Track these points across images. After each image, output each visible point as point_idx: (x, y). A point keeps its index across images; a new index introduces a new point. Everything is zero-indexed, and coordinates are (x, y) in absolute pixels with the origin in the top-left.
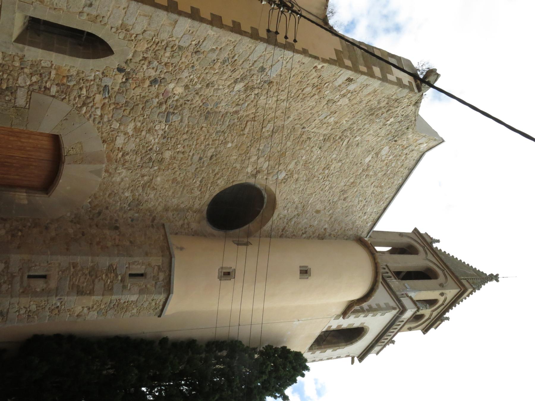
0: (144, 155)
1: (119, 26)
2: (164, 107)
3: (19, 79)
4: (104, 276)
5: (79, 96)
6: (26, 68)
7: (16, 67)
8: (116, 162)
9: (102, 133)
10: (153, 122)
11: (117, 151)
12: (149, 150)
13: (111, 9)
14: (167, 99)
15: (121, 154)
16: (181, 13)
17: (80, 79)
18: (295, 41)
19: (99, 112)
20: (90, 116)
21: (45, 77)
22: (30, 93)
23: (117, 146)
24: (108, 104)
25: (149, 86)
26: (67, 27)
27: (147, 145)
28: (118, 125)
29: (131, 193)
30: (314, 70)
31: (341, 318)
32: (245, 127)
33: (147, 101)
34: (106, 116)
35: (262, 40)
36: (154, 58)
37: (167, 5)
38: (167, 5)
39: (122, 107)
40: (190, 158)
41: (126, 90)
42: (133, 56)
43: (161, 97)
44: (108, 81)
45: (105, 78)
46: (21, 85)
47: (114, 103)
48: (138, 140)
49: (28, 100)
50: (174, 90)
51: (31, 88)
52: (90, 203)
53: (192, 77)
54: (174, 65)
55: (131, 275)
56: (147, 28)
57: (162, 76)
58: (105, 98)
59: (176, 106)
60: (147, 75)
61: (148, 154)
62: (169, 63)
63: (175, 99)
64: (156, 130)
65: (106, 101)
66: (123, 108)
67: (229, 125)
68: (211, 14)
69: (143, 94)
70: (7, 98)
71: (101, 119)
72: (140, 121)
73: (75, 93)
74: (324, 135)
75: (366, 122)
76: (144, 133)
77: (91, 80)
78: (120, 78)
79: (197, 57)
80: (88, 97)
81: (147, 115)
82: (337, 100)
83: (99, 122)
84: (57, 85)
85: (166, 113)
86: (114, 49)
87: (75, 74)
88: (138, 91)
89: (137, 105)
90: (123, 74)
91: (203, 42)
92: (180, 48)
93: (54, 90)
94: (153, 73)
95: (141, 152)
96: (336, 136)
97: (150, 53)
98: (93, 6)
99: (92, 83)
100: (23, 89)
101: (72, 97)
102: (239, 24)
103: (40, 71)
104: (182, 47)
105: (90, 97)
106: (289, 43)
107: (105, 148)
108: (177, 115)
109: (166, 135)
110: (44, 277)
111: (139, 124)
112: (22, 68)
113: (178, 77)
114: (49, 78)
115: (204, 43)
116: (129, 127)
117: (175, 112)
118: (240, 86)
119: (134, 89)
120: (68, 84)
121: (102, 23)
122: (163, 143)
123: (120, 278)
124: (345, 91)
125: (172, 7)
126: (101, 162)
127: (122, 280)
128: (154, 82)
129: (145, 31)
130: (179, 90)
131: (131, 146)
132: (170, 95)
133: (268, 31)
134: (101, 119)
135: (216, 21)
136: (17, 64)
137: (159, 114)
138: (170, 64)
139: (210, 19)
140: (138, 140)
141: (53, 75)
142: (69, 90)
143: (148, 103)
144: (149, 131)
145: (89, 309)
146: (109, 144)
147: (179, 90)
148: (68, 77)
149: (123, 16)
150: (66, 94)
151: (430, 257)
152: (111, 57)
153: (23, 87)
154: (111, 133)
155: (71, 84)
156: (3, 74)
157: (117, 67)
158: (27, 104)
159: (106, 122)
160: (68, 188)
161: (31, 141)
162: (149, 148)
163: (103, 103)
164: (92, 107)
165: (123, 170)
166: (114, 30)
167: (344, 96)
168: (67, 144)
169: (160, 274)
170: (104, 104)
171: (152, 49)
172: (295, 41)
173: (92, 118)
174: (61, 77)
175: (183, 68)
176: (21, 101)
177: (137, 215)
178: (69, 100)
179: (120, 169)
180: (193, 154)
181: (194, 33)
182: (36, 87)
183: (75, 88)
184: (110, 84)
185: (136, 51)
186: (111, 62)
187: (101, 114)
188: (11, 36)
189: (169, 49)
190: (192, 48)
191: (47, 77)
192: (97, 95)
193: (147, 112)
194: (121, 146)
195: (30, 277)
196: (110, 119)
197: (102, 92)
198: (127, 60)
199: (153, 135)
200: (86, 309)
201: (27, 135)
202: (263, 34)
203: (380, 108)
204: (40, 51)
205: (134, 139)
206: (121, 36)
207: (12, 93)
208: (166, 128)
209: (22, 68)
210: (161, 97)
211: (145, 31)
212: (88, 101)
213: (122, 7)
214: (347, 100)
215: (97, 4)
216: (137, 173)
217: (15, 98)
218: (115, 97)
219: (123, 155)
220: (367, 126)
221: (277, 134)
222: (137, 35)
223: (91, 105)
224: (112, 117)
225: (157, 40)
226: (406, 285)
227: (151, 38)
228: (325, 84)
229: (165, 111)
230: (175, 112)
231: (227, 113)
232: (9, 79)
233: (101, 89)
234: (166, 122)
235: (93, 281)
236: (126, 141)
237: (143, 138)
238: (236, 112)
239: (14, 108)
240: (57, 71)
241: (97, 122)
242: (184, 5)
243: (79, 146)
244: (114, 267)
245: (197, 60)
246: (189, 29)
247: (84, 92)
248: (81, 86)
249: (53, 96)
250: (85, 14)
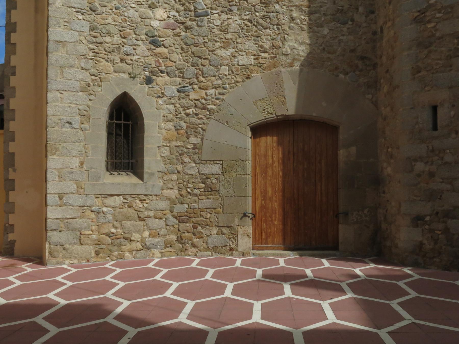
0: (260, 27)
1: (86, 93)
2: (189, 23)
3: (190, 173)
4: (430, 26)
5: (197, 115)
6: (177, 168)
7: (178, 177)
8: (276, 57)
9: (237, 82)
10: (211, 29)
11: (260, 60)
12: (251, 23)
13: (66, 105)
14: (179, 23)
15: (263, 55)
17: (177, 118)
19: (212, 92)
20: (217, 99)
21: (182, 150)
22: (203, 162)
23: (253, 62)
24: (199, 84)
25: (165, 47)
27: (245, 27)
28: (223, 67)
29: (322, 26)
33: (186, 44)
34: (215, 83)
36: (119, 51)
39: (199, 69)
41: (178, 69)
42: (124, 73)
43: (178, 30)
44: (172, 90)
45: (166, 94)
47: (197, 78)
48: (239, 40)
49: (212, 162)
50: (161, 19)
51: (198, 161)
52: (346, 74)
53: (133, 5)
54: (121, 29)
56: (78, 68)
57: (143, 37)
58: (193, 88)
59: (185, 10)
60: (147, 53)
61: (257, 22)
62: (121, 35)
63: (177, 14)
64: (222, 23)
65: (196, 87)
66: (201, 67)
69: (179, 51)
70: (214, 182)
71: (220, 87)
72: (214, 45)
73: (194, 120)
76: (229, 36)
77: (175, 107)
79: (100, 8)
80: (196, 106)
81: (204, 39)
83: (224, 88)
84: (188, 139)
85: (197, 19)
87: (171, 123)
88: (175, 57)
89: (193, 53)
91: (74, 8)
92: (92, 29)
93: (193, 140)
94: (143, 48)
95: (256, 32)
97: (112, 58)
98: (69, 120)
99: (178, 105)
100: (201, 169)
101: (199, 121)
103: (177, 156)
104: (90, 27)
105: (195, 104)
107: (258, 74)
108: (197, 6)
109: (226, 9)
111: (218, 44)
113: (140, 20)
114: (183, 147)
115: (75, 6)
116: (224, 55)
119: (175, 62)
120: (185, 128)
121: (88, 109)
122: (238, 9)
126: (279, 74)
128: (155, 43)
129: (83, 69)
130: (160, 13)
131: (251, 46)
132: (172, 21)
134: (220, 87)
136: (175, 177)
138: (122, 33)
140: (239, 40)
141: (179, 144)
142: (191, 126)
143: (188, 42)
144: (225, 31)
146: (252, 71)
148: (177, 130)
149: (71, 93)
150: (196, 129)
152: (132, 93)
153: (199, 169)
154: (235, 73)
156: (188, 188)
157: (145, 85)
158: (217, 163)
159: (223, 82)
160: (324, 104)
161: (270, 153)
162: (249, 24)
163: (199, 90)
164: (205, 100)
165: (286, 46)
166: (92, 97)
168: (259, 116)
170: (200, 88)
171: (106, 56)
173: (221, 97)
174: (178, 135)
175: (123, 18)
176: (216, 169)
177: (361, 9)
178: (204, 123)
179: (284, 50)
181: (67, 20)
182: (196, 157)
183: (188, 121)
184: (174, 88)
185: (115, 71)
186: (139, 93)
187: (213, 88)
188: (135, 185)
189: (99, 40)
190: (88, 16)
191: (181, 148)
192: (191, 97)
193: (201, 40)
194: (253, 57)
195: (435, 128)
196: (217, 77)
197: (186, 93)
198: (131, 77)
199: (229, 24)
201: (263, 158)
205: (239, 46)
207: (208, 178)
208: (217, 12)
209: (178, 172)
210: (178, 30)
211: (83, 69)
212: (199, 105)
213: (60, 95)
215: (65, 117)
216: (289, 27)
217: (213, 174)
218: (190, 79)
219: (265, 52)
222: (91, 75)
223: (204, 101)
224: (214, 76)
225: (91, 54)
227: (90, 61)
229: (194, 20)
230: (192, 8)
232: (193, 182)
233: (183, 95)
234: (208, 15)
235: (439, 38)
236: (244, 53)
237: (235, 35)
239: (225, 174)
240: (172, 140)
241: (224, 91)
243: (259, 103)
244: (417, 14)
245: (105, 6)
246: (62, 27)
247: (190, 111)
248: (185, 116)
249: (202, 139)
250: (82, 126)
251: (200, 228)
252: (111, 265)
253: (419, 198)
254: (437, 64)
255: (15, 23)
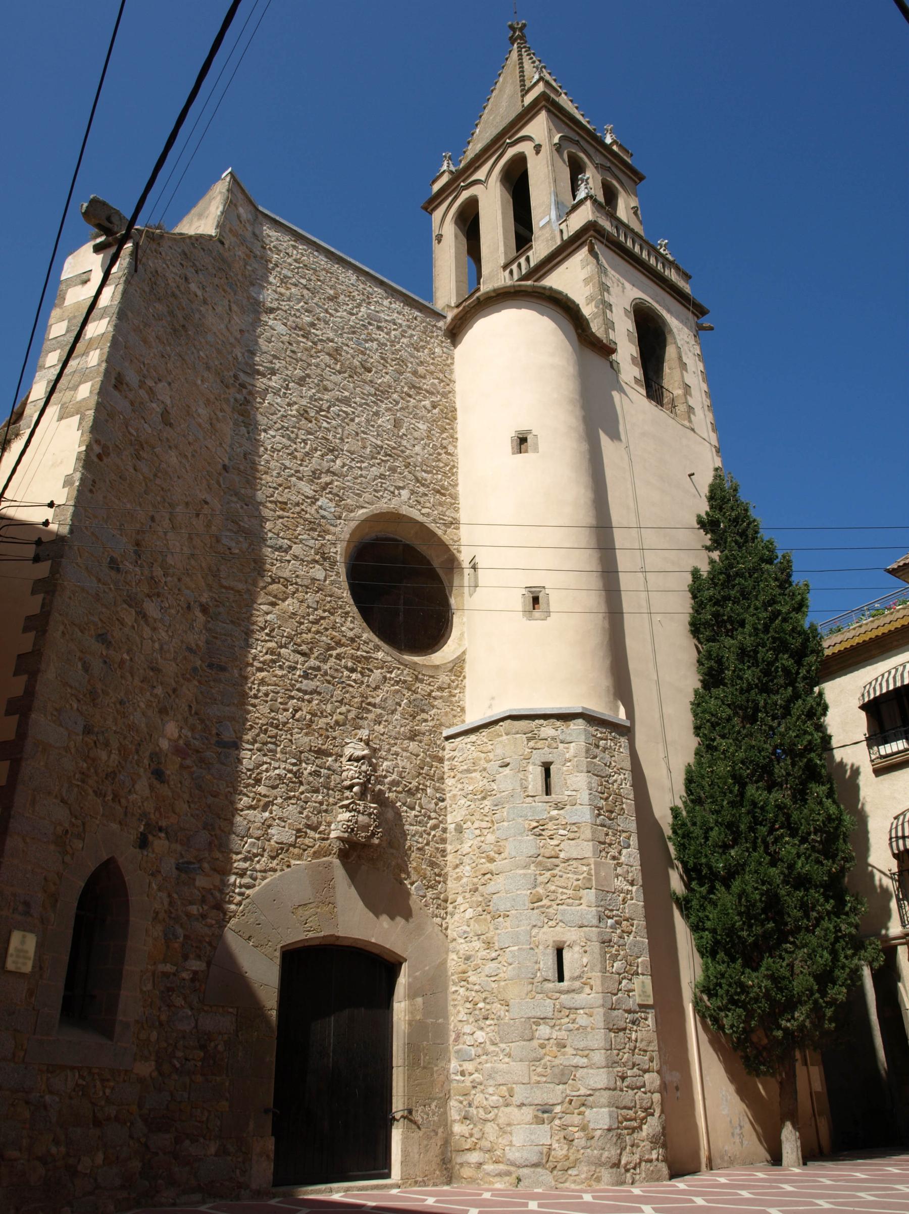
16: (22, 734)
18: (51, 505)
26: (72, 948)
30: (105, 460)
31: (614, 356)
32: (232, 589)
35: (55, 570)
36: (113, 779)
37: (8, 762)
38: (8, 762)
40: (307, 697)
44: (168, 866)
46: (193, 1025)
55: (548, 791)
56: (56, 797)
67: (232, 622)
68: (15, 675)
70: (221, 1048)
74: (236, 424)
75: (203, 340)
78: (160, 844)
81: (228, 786)
82: (162, 406)
86: (105, 857)
90: (150, 838)
91: (71, 687)
93: (196, 965)
94: (142, 786)
96: (236, 400)
102: (28, 618)
104: (85, 726)
106: (55, 516)
110: (559, 952)
112: (161, 1024)
117: (214, 731)
118: (151, 608)
123: (554, 813)
124: (142, 392)
125: (13, 751)
127: (559, 806)
129: (63, 801)
133: (37, 559)
135: (28, 664)
137: (223, 764)
139: (24, 678)
141: (169, 968)
145: (619, 865)
147: (171, 729)
151: (481, 175)
153: (197, 1021)
155: (180, 931)
157: (138, 850)
167: (151, 392)
169: (543, 736)
172: (51, 505)
180: (299, 690)
186: (129, 860)
200: (619, 870)
202: (43, 569)
203: (171, 313)
204: (123, 993)
206: (78, 844)
209: (161, 1024)
210: (188, 762)
214: (160, 385)
220: (210, 338)
221: (242, 524)
226: (542, 223)
228: (130, 433)
231: (209, 630)
238: (204, 609)
242: (0, 728)
244: (535, 824)
247: (194, 909)
249: (209, 964)
251: (187, 1142)
252: (209, 1208)
253: (544, 1079)
254: (562, 893)
255: (16, 674)
